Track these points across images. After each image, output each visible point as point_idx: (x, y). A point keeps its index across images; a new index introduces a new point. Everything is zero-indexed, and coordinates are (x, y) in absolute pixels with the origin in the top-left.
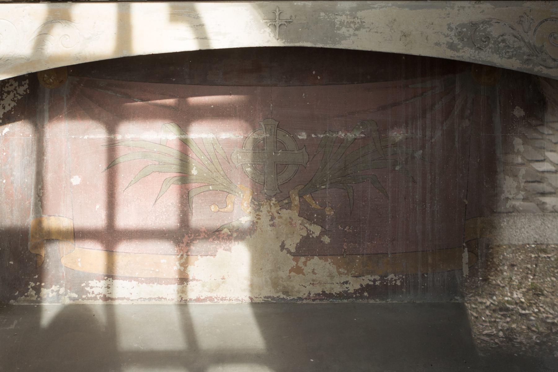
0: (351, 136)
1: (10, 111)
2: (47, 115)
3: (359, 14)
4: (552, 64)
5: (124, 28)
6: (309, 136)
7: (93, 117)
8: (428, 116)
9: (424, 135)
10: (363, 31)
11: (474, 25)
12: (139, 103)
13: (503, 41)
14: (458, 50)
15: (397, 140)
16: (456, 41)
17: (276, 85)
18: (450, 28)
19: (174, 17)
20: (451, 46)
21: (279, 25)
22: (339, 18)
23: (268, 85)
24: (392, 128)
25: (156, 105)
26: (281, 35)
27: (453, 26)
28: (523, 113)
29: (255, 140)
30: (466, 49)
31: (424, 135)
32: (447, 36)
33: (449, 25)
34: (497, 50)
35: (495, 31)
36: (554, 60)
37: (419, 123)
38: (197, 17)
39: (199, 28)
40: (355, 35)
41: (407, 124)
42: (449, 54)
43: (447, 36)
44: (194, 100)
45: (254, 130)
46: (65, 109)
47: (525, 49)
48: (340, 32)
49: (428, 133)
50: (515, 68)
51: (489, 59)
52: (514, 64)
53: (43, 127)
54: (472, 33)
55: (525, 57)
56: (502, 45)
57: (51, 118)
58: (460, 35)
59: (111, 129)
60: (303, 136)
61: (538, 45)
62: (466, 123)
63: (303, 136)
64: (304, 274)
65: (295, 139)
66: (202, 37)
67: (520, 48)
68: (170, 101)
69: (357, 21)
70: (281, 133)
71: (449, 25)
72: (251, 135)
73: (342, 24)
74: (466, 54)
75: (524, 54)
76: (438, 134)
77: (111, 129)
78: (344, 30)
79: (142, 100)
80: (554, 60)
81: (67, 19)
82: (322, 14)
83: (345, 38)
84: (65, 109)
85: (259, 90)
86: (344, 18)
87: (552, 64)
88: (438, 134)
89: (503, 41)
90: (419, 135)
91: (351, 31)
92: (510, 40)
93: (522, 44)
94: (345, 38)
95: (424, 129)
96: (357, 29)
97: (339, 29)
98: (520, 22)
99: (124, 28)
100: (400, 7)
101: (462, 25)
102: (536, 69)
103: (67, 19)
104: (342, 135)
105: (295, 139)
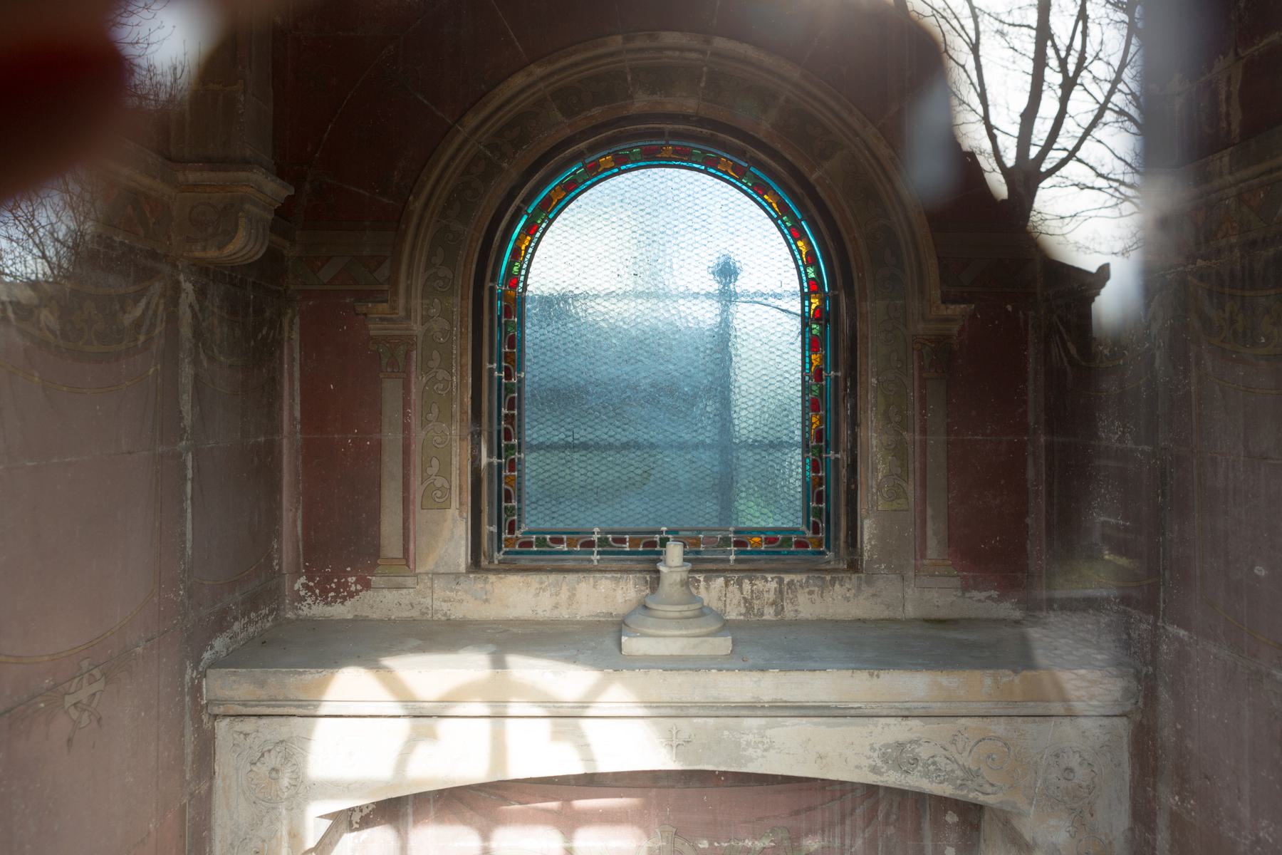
0: (758, 845)
1: (368, 815)
2: (411, 819)
3: (768, 732)
4: (990, 789)
5: (498, 749)
6: (711, 844)
7: (464, 822)
8: (848, 822)
9: (843, 844)
10: (772, 752)
11: (900, 746)
12: (517, 807)
13: (934, 763)
14: (881, 774)
15: (812, 849)
16: (880, 764)
17: (673, 787)
18: (873, 749)
19: (556, 735)
20: (874, 770)
21: (679, 745)
22: (745, 737)
23: (664, 787)
24: (807, 835)
25: (537, 809)
26: (678, 757)
27: (877, 746)
28: (956, 819)
29: (650, 849)
30: (891, 772)
31: (843, 844)
32: (869, 758)
33: (871, 745)
34: (926, 774)
35: (924, 752)
36: (992, 785)
37: (838, 830)
38: (582, 736)
39: (584, 747)
40: (763, 757)
41: (823, 831)
42: (871, 779)
43: (869, 758)
44: (580, 804)
45: (649, 838)
46: (432, 813)
47: (959, 773)
48: (747, 753)
49: (847, 842)
50: (947, 795)
51: (917, 784)
52: (946, 790)
53: (406, 833)
54: (899, 755)
55: (959, 782)
56: (932, 768)
57: (415, 823)
58: (885, 758)
59: (485, 836)
60: (704, 844)
61: (974, 768)
62: (891, 830)
63: (704, 844)
64: (685, 584)
65: (695, 848)
66: (589, 759)
67: (953, 771)
68: (553, 805)
69: (765, 740)
70: (679, 842)
71: (871, 745)
72: (646, 844)
73: (748, 744)
74: (892, 778)
75: (957, 778)
76: (859, 842)
77: (485, 836)
78: (751, 751)
79: (520, 803)
80: (992, 785)
81: (432, 736)
82: (726, 733)
83: (752, 760)
84: (432, 813)
85: (654, 792)
86: (750, 737)
87: (990, 789)
88: (859, 842)
89: (934, 763)
90: (837, 843)
91: (759, 752)
92: (942, 761)
93: (955, 766)
94: (752, 760)
95: (843, 837)
96: (765, 750)
97: (745, 750)
98: (953, 742)
99: (498, 749)
100: (815, 724)
101: (887, 746)
102: (971, 795)
103: (432, 736)
104: (748, 843)
105: (695, 848)
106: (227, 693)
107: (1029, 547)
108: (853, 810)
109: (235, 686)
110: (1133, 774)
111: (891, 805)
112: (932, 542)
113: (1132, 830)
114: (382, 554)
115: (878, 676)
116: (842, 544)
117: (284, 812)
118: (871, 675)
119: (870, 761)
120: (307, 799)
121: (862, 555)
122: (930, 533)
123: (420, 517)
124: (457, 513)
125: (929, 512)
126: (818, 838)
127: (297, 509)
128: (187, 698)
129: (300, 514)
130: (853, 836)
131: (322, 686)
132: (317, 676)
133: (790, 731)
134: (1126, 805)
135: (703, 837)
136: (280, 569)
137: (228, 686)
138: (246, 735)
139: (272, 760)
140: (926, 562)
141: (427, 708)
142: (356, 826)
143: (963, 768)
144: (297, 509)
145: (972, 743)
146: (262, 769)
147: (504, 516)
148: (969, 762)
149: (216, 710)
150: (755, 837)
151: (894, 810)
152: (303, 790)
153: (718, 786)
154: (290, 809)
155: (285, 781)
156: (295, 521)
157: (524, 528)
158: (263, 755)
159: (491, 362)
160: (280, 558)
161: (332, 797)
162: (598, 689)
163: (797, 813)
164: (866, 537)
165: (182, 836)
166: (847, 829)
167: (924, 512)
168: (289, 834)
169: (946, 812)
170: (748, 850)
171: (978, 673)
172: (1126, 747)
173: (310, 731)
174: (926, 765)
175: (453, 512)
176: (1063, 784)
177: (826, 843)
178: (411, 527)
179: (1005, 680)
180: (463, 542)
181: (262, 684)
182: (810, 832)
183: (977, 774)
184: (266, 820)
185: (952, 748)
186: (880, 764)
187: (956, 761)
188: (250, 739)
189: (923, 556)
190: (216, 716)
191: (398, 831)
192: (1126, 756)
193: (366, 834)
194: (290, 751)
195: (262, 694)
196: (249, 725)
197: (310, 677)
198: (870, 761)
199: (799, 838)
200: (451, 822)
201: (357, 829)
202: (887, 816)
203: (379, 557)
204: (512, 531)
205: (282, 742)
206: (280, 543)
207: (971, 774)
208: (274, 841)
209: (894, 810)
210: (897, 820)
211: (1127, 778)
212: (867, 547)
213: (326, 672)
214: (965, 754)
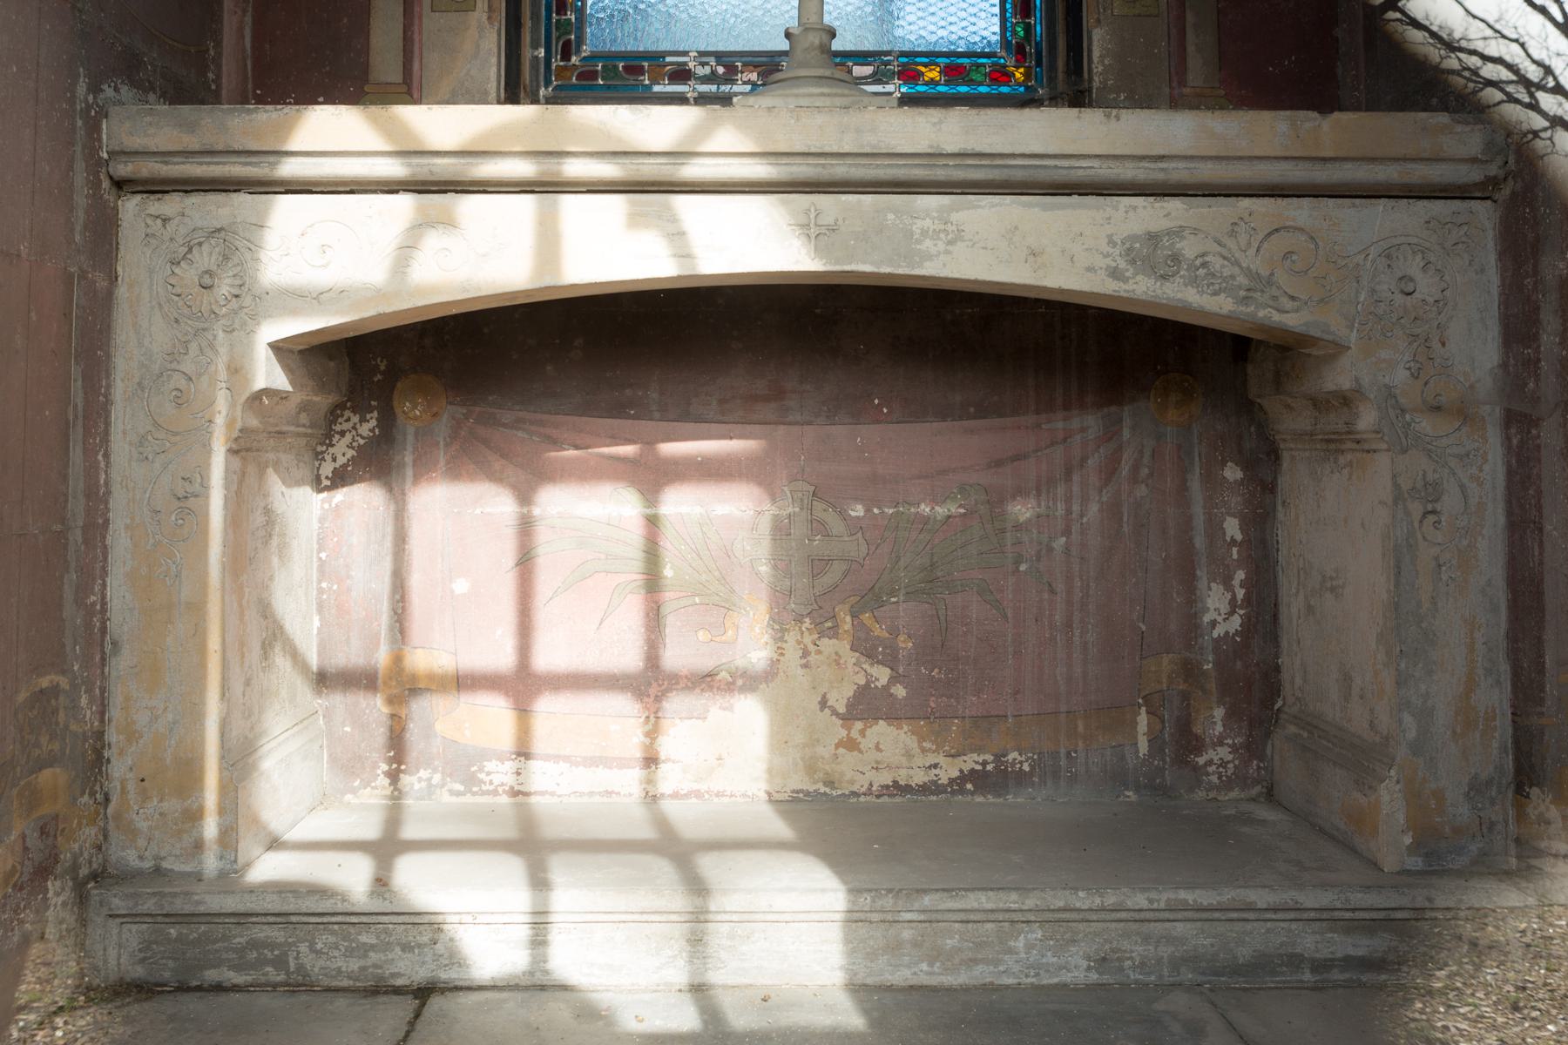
0: (941, 511)
1: (345, 466)
2: (409, 472)
3: (955, 217)
4: (1288, 305)
5: (548, 240)
6: (868, 510)
7: (495, 477)
8: (1076, 478)
9: (1069, 512)
11: (1153, 238)
14: (1125, 280)
16: (1122, 265)
17: (810, 423)
19: (636, 220)
20: (1115, 273)
21: (817, 234)
22: (919, 223)
24: (1014, 497)
25: (603, 456)
26: (819, 251)
27: (1117, 239)
28: (1239, 475)
31: (1069, 512)
32: (1107, 256)
34: (1193, 281)
35: (1189, 248)
36: (1293, 298)
37: (1061, 490)
38: (674, 219)
39: (677, 237)
40: (947, 252)
43: (1107, 256)
46: (442, 462)
47: (1242, 280)
48: (923, 247)
49: (1076, 508)
51: (1179, 296)
53: (404, 494)
55: (1242, 293)
57: (417, 479)
58: (1131, 256)
59: (525, 497)
60: (858, 511)
61: (1265, 273)
62: (1142, 491)
63: (858, 511)
66: (685, 255)
67: (1233, 277)
69: (950, 228)
73: (924, 233)
75: (1240, 287)
76: (1094, 508)
77: (525, 497)
78: (928, 243)
79: (577, 447)
80: (1293, 298)
82: (891, 216)
83: (929, 257)
86: (928, 222)
90: (1061, 507)
91: (941, 246)
92: (1216, 263)
93: (1237, 270)
94: (929, 257)
95: (1068, 500)
96: (950, 243)
97: (919, 242)
98: (1233, 233)
99: (548, 240)
101: (1133, 238)
102: (1261, 314)
104: (925, 509)
106: (136, 142)
107: (1340, 71)
108: (1084, 460)
109: (152, 131)
110: (1503, 279)
111: (1141, 452)
112: (1195, 62)
113: (1504, 365)
114: (371, 78)
115: (1118, 118)
116: (1061, 76)
117: (221, 335)
118: (1108, 116)
119: (1108, 261)
120: (256, 318)
121: (1091, 80)
122: (1191, 49)
123: (431, 23)
124: (485, 16)
125: (1190, 18)
126: (1032, 502)
127: (244, 11)
128: (79, 123)
129: (248, 19)
130: (1085, 500)
131: (286, 129)
132: (274, 115)
133: (987, 217)
134: (1494, 332)
135: (857, 499)
136: (219, 87)
137: (145, 131)
138: (165, 220)
139: (205, 258)
140: (1186, 91)
141: (444, 168)
142: (327, 483)
143: (1248, 272)
144: (244, 11)
145: (1261, 236)
146: (189, 274)
147: (554, 34)
148: (1258, 265)
149: (123, 169)
150: (935, 501)
151: (1146, 460)
152: (250, 302)
153: (878, 422)
154: (229, 331)
155: (224, 288)
156: (241, 29)
157: (586, 50)
158: (190, 250)
159: (535, 46)
160: (219, 67)
161: (294, 312)
162: (702, 131)
163: (999, 463)
164: (1096, 54)
165: (67, 315)
166: (1076, 489)
167: (1181, 18)
168: (228, 368)
169: (1224, 463)
170: (926, 520)
171: (1267, 115)
172: (1491, 245)
173: (264, 214)
174: (1192, 267)
175: (480, 14)
176: (1399, 299)
177: (1042, 510)
178: (416, 37)
179: (1308, 125)
180: (494, 60)
181: (191, 127)
182: (1019, 492)
183: (1270, 282)
184: (193, 347)
185: (1231, 243)
186: (1122, 265)
187: (1237, 263)
188: (171, 227)
189: (1182, 83)
190: (120, 185)
191: (390, 489)
192: (1492, 258)
193: (340, 495)
194: (233, 247)
195: (193, 143)
196: (170, 205)
197: (265, 116)
198: (1108, 261)
199: (1002, 502)
200: (472, 478)
201: (328, 489)
202: (1135, 468)
203: (367, 81)
204: (566, 56)
205: (219, 230)
206: (218, 44)
207: (1259, 283)
208: (205, 379)
209: (1146, 460)
210: (1151, 475)
211: (1495, 291)
212: (1098, 68)
213: (289, 110)
214: (1252, 252)
